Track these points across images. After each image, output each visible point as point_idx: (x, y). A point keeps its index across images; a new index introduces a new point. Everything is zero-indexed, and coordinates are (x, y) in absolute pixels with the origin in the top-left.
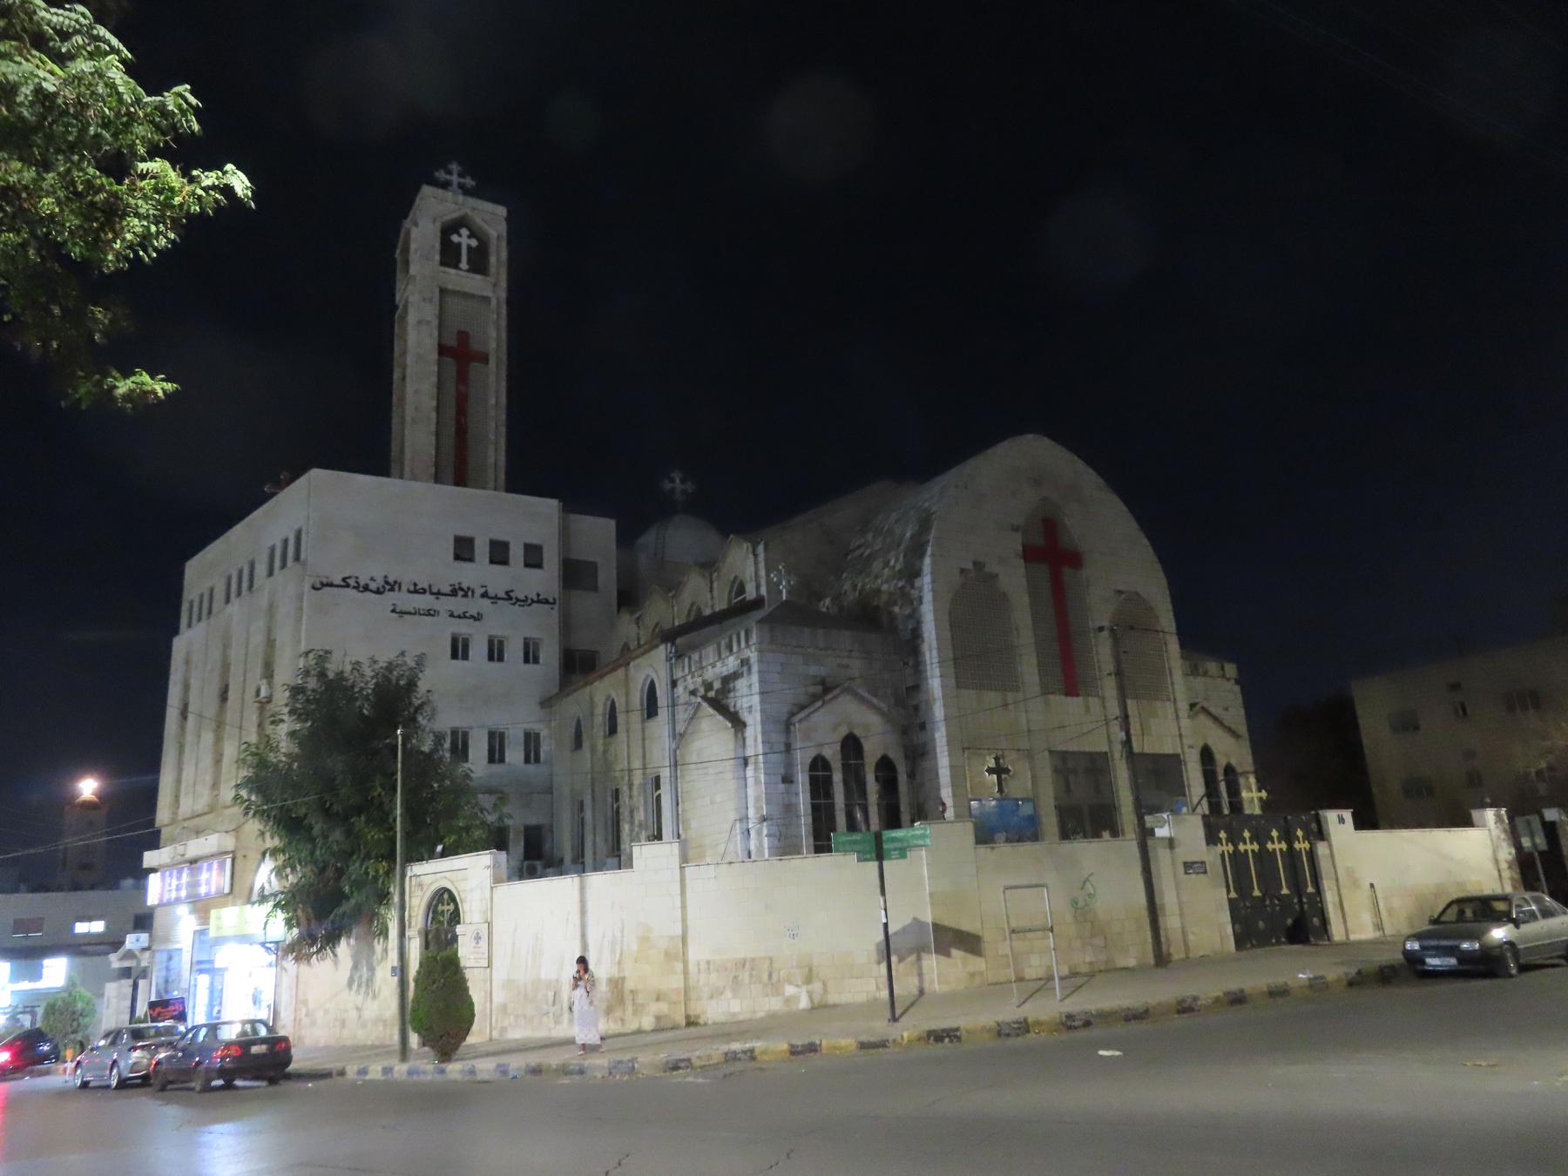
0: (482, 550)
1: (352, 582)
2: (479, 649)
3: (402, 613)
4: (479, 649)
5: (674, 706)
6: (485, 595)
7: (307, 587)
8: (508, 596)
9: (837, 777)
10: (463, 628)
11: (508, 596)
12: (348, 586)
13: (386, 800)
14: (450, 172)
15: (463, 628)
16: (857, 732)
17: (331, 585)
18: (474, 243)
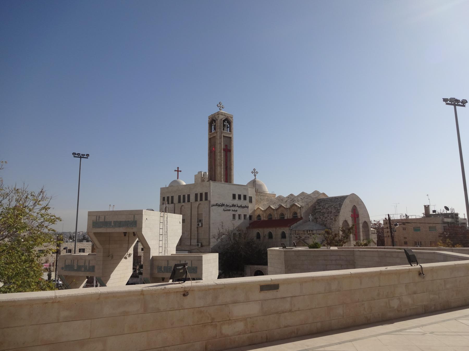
2: (237, 217)
4: (237, 217)
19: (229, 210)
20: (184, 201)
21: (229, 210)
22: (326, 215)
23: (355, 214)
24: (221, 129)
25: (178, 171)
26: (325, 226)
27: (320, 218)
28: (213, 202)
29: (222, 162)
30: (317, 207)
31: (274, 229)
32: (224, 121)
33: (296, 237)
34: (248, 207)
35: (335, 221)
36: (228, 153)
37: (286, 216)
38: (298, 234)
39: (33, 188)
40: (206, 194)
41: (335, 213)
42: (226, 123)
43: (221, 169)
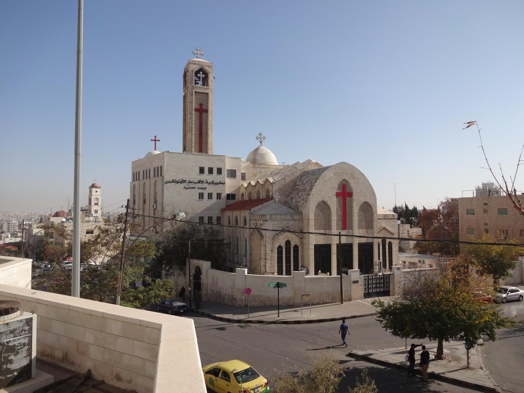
0: (206, 171)
2: (206, 196)
3: (187, 188)
4: (206, 196)
6: (207, 182)
9: (284, 250)
11: (213, 183)
15: (201, 191)
16: (290, 239)
18: (204, 76)
19: (194, 188)
20: (158, 176)
21: (194, 188)
23: (345, 193)
24: (192, 83)
25: (155, 140)
28: (167, 178)
29: (193, 126)
31: (239, 212)
32: (197, 72)
34: (224, 184)
35: (306, 202)
36: (204, 114)
39: (325, 154)
40: (161, 167)
42: (201, 75)
43: (192, 135)
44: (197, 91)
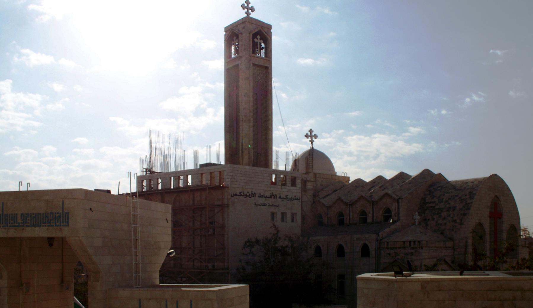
1: (242, 194)
5: (446, 247)
6: (280, 197)
7: (230, 197)
8: (286, 198)
10: (273, 209)
12: (241, 195)
13: (505, 266)
14: (257, 39)
15: (273, 209)
17: (236, 195)
22: (444, 214)
26: (442, 233)
27: (433, 219)
30: (428, 199)
33: (389, 254)
35: (461, 224)
37: (370, 215)
38: (392, 249)
41: (461, 209)
44: (256, 63)
